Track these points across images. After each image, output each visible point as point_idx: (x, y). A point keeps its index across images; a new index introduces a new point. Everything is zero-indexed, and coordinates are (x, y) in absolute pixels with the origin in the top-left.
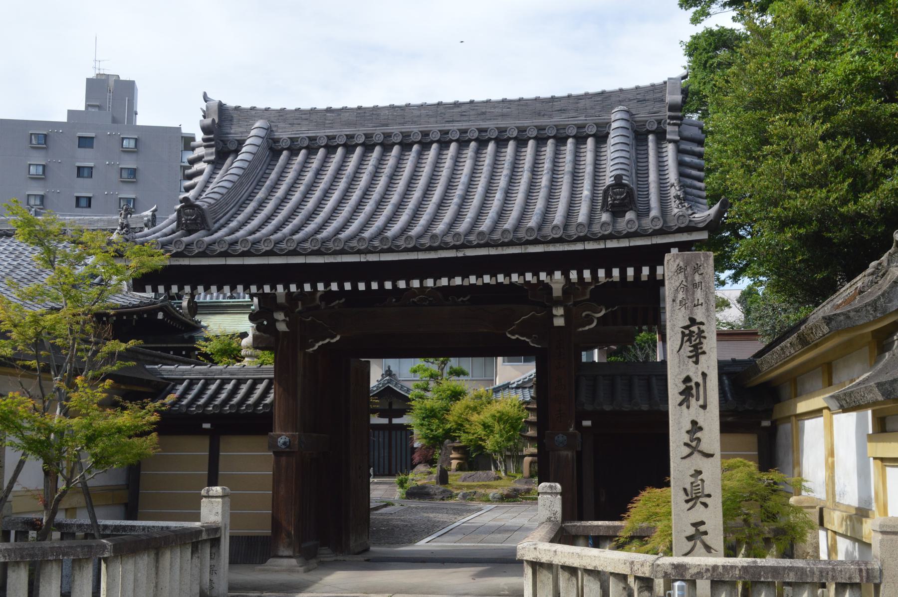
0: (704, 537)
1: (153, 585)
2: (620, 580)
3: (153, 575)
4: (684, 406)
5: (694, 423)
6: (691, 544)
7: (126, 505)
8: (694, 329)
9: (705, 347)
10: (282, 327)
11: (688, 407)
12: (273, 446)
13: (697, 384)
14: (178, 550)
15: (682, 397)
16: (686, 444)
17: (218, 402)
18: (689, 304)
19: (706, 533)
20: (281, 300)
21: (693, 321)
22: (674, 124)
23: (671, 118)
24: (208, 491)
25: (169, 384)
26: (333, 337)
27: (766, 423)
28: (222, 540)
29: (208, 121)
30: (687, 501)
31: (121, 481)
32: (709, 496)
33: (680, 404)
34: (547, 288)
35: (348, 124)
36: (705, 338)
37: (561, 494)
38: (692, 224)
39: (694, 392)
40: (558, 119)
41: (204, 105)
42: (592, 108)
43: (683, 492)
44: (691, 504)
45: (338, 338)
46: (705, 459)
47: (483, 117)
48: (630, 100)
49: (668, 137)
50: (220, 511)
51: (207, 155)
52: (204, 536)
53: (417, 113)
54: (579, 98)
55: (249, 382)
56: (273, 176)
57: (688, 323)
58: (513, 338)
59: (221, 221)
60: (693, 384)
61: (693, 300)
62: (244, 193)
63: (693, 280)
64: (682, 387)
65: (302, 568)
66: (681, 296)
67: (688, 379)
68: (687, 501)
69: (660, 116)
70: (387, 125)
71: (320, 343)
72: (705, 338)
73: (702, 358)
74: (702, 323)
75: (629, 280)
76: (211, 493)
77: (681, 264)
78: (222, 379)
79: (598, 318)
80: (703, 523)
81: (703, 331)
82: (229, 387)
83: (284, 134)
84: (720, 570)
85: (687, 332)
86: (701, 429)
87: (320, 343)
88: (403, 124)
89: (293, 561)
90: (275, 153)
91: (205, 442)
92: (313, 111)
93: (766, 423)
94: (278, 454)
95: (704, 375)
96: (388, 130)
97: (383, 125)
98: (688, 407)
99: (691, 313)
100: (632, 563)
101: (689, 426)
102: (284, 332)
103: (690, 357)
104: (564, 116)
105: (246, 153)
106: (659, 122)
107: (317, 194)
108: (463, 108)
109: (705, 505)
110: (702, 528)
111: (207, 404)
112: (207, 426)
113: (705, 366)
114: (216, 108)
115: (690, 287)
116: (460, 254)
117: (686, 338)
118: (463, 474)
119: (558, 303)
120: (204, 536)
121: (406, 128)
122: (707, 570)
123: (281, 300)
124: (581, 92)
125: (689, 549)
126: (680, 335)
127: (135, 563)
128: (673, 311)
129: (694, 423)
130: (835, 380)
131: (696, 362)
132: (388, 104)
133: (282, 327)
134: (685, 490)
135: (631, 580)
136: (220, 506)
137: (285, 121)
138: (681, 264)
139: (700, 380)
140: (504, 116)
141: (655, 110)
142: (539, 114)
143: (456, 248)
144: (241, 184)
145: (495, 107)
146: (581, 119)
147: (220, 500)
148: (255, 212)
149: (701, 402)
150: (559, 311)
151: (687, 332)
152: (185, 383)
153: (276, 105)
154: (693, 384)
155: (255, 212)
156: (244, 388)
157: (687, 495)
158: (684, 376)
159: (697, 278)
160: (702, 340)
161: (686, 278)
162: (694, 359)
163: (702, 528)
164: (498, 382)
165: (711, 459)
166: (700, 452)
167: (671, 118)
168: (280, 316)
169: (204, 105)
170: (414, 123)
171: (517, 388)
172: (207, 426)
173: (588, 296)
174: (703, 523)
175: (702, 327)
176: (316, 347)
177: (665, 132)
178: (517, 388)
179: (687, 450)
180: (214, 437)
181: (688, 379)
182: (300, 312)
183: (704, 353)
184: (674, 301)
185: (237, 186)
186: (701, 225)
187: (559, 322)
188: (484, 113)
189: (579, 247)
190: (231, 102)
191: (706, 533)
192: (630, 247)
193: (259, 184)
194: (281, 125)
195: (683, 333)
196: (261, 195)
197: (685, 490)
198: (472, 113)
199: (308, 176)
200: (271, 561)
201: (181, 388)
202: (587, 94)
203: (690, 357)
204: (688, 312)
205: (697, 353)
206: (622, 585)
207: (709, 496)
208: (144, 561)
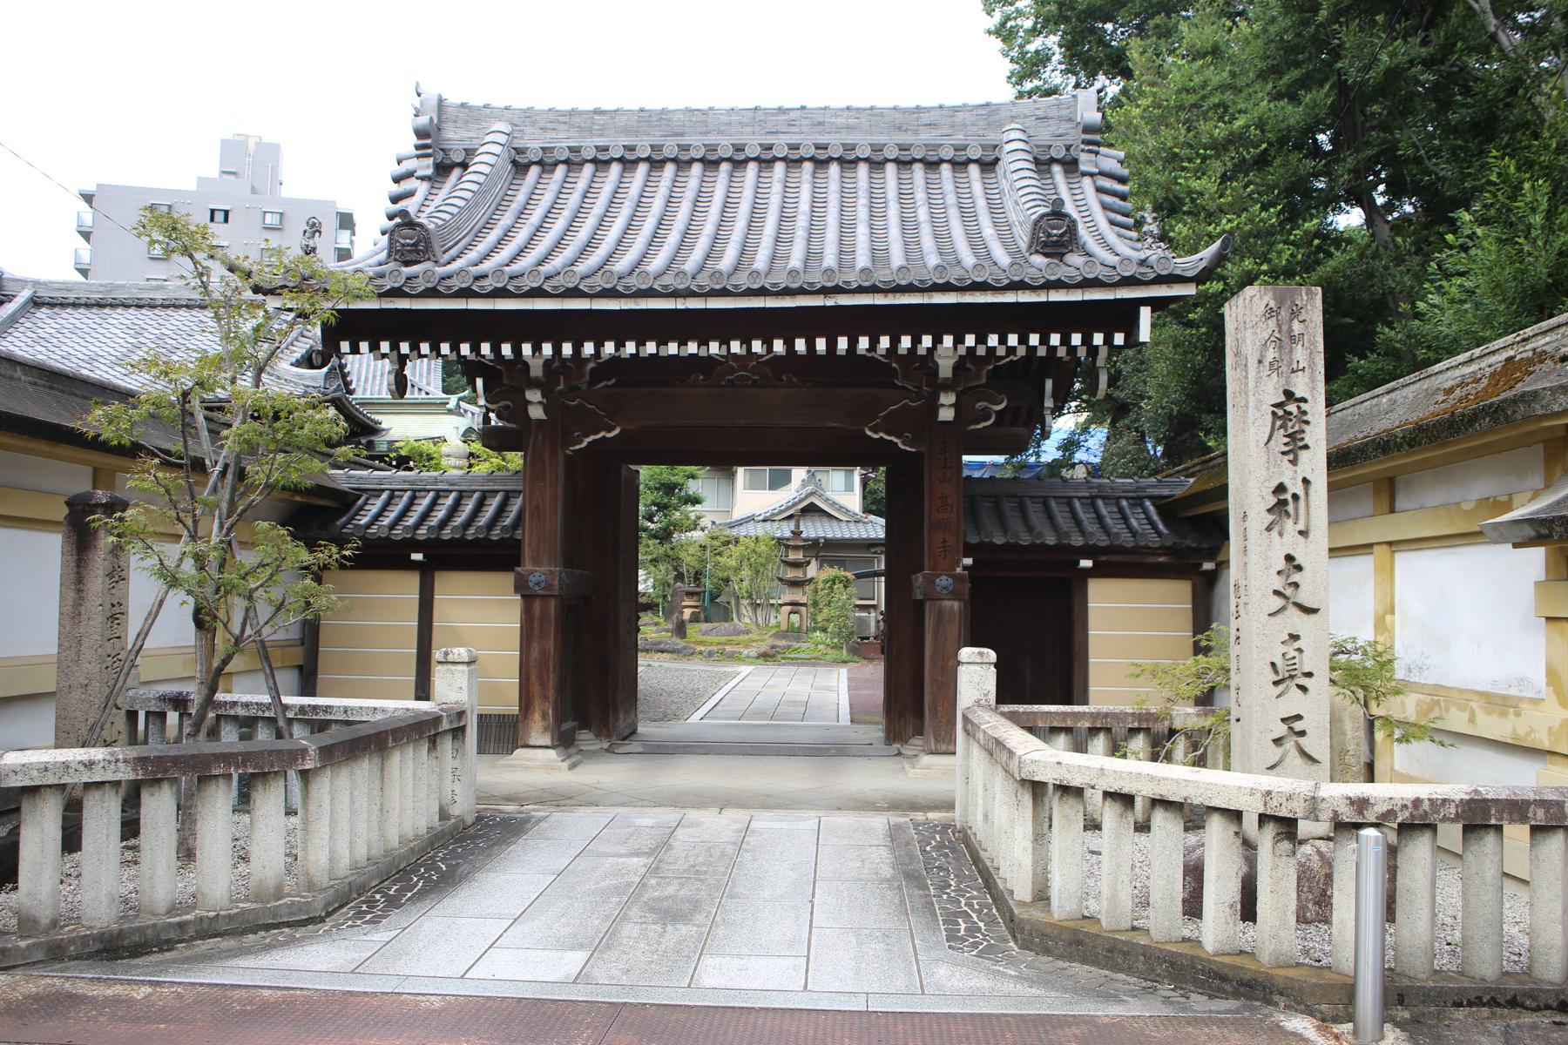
0: (1301, 740)
1: (376, 808)
2: (1231, 820)
3: (377, 792)
4: (1274, 533)
5: (1289, 558)
6: (1279, 751)
7: (300, 668)
8: (1292, 408)
9: (1308, 439)
10: (536, 413)
11: (1281, 534)
12: (520, 586)
13: (1295, 497)
14: (411, 749)
15: (1271, 518)
16: (1276, 593)
17: (434, 521)
18: (1284, 369)
19: (1302, 733)
20: (536, 369)
21: (1289, 394)
22: (1090, 151)
23: (1085, 142)
24: (446, 654)
25: (359, 497)
26: (613, 429)
27: (1208, 566)
28: (468, 729)
29: (423, 120)
30: (1276, 683)
31: (294, 634)
32: (1309, 675)
33: (1269, 529)
34: (927, 363)
35: (627, 131)
36: (1307, 423)
37: (996, 666)
38: (1178, 272)
39: (1290, 508)
40: (926, 136)
41: (417, 102)
42: (973, 124)
43: (1270, 669)
44: (1281, 687)
45: (617, 431)
46: (1305, 617)
47: (820, 128)
48: (1026, 117)
49: (1082, 168)
50: (465, 685)
51: (422, 168)
52: (445, 725)
53: (725, 119)
54: (955, 110)
55: (476, 495)
56: (521, 197)
57: (1282, 398)
58: (876, 436)
59: (453, 252)
60: (1288, 496)
61: (1290, 363)
62: (481, 215)
63: (1290, 329)
64: (1272, 500)
65: (566, 764)
66: (1271, 354)
67: (1281, 488)
68: (1276, 683)
69: (1068, 140)
70: (682, 135)
71: (592, 438)
72: (1307, 423)
73: (1303, 455)
74: (1304, 400)
75: (942, 375)
76: (450, 658)
77: (1272, 304)
78: (438, 491)
79: (998, 413)
80: (1299, 717)
81: (1305, 413)
82: (449, 501)
83: (534, 143)
84: (1426, 806)
85: (1280, 413)
86: (1299, 568)
87: (592, 438)
88: (705, 133)
89: (552, 753)
90: (520, 168)
91: (413, 581)
92: (573, 113)
93: (1208, 566)
94: (528, 598)
95: (1306, 481)
96: (685, 141)
97: (676, 135)
98: (1281, 534)
99: (1288, 382)
100: (1269, 793)
101: (1281, 564)
102: (539, 421)
103: (1284, 453)
104: (939, 132)
105: (481, 166)
106: (1068, 148)
107: (591, 221)
108: (792, 115)
109: (1303, 689)
110: (1298, 726)
111: (418, 525)
112: (417, 557)
113: (1308, 468)
114: (435, 102)
115: (1286, 340)
116: (830, 302)
117: (1278, 423)
118: (704, 626)
119: (947, 386)
120: (445, 725)
121: (711, 139)
122: (1405, 806)
123: (536, 369)
124: (958, 102)
125: (1277, 759)
126: (1270, 417)
127: (352, 774)
128: (1258, 379)
129: (1289, 558)
130: (1399, 505)
131: (1294, 462)
132: (682, 107)
133: (536, 413)
134: (1273, 664)
135: (1250, 824)
136: (466, 677)
137: (533, 124)
138: (1272, 304)
139: (1300, 491)
140: (849, 128)
141: (1060, 131)
142: (900, 129)
143: (825, 291)
144: (477, 204)
145: (837, 116)
146: (959, 139)
147: (465, 668)
148: (500, 243)
149: (1301, 526)
150: (947, 399)
151: (1280, 413)
152: (385, 496)
153: (520, 103)
154: (1288, 496)
155: (500, 243)
156: (469, 506)
157: (1276, 672)
158: (1275, 484)
159: (1297, 327)
160: (1305, 427)
161: (1279, 326)
162: (1291, 457)
163: (1298, 726)
164: (738, 514)
165: (1313, 617)
166: (1296, 604)
167: (1085, 142)
168: (534, 396)
169: (417, 102)
170: (720, 132)
171: (764, 521)
172: (417, 557)
173: (984, 381)
174: (1299, 717)
175: (1304, 406)
176: (584, 445)
177: (1075, 162)
178: (764, 521)
179: (1278, 602)
180: (427, 572)
181: (1281, 488)
182: (560, 392)
183: (1306, 447)
184: (1260, 362)
185: (471, 206)
186: (1190, 274)
187: (946, 415)
188: (820, 124)
189: (1009, 298)
190: (453, 98)
191: (1302, 733)
192: (1083, 302)
193: (499, 207)
194: (529, 130)
195: (1274, 413)
196: (506, 220)
197: (1273, 664)
198: (805, 122)
199: (574, 199)
200: (518, 752)
201: (378, 503)
202: (965, 105)
203: (1284, 453)
204: (1282, 381)
205: (1295, 446)
206: (1233, 828)
207: (1309, 675)
208: (364, 769)
